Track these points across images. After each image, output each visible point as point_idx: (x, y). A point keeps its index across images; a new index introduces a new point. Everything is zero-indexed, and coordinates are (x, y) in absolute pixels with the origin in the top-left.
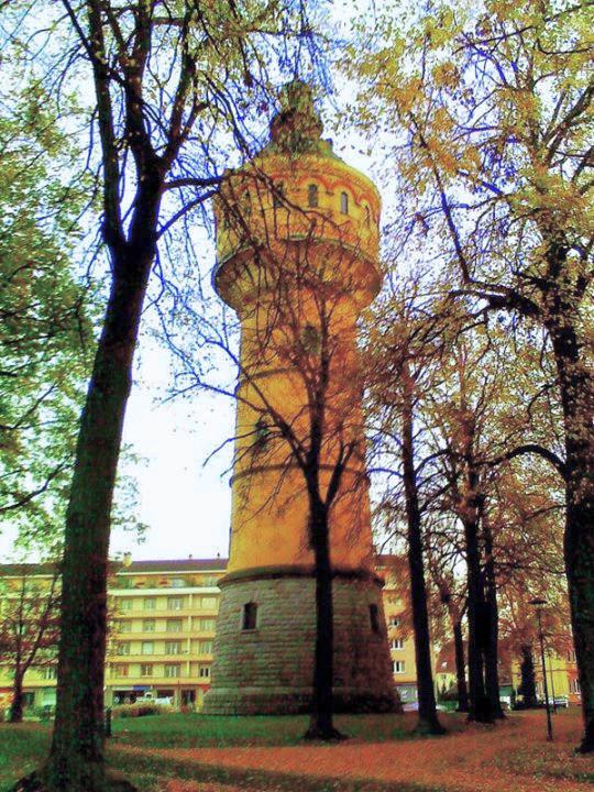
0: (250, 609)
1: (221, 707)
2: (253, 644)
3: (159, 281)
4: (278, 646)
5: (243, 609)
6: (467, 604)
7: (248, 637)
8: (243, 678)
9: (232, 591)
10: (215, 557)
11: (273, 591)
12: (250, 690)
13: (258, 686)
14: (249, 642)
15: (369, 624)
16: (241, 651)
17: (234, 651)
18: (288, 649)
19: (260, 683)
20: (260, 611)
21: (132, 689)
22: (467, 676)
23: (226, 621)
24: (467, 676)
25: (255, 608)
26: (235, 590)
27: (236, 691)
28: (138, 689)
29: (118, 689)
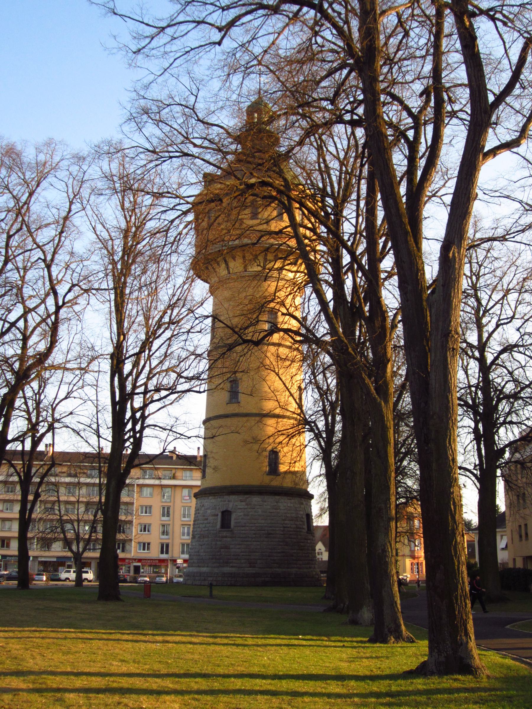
0: (226, 515)
1: (205, 580)
2: (229, 539)
3: (170, 336)
4: (247, 541)
5: (220, 514)
6: (340, 95)
7: (225, 534)
8: (221, 561)
9: (209, 502)
10: (110, 430)
11: (244, 503)
12: (227, 570)
13: (232, 567)
14: (226, 537)
15: (305, 527)
16: (219, 543)
17: (214, 543)
18: (255, 543)
19: (235, 565)
20: (233, 516)
21: (55, 560)
22: (428, 315)
23: (206, 521)
24: (428, 315)
25: (230, 515)
26: (213, 501)
27: (216, 570)
28: (60, 560)
29: (43, 559)
